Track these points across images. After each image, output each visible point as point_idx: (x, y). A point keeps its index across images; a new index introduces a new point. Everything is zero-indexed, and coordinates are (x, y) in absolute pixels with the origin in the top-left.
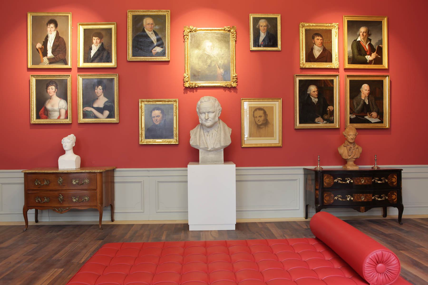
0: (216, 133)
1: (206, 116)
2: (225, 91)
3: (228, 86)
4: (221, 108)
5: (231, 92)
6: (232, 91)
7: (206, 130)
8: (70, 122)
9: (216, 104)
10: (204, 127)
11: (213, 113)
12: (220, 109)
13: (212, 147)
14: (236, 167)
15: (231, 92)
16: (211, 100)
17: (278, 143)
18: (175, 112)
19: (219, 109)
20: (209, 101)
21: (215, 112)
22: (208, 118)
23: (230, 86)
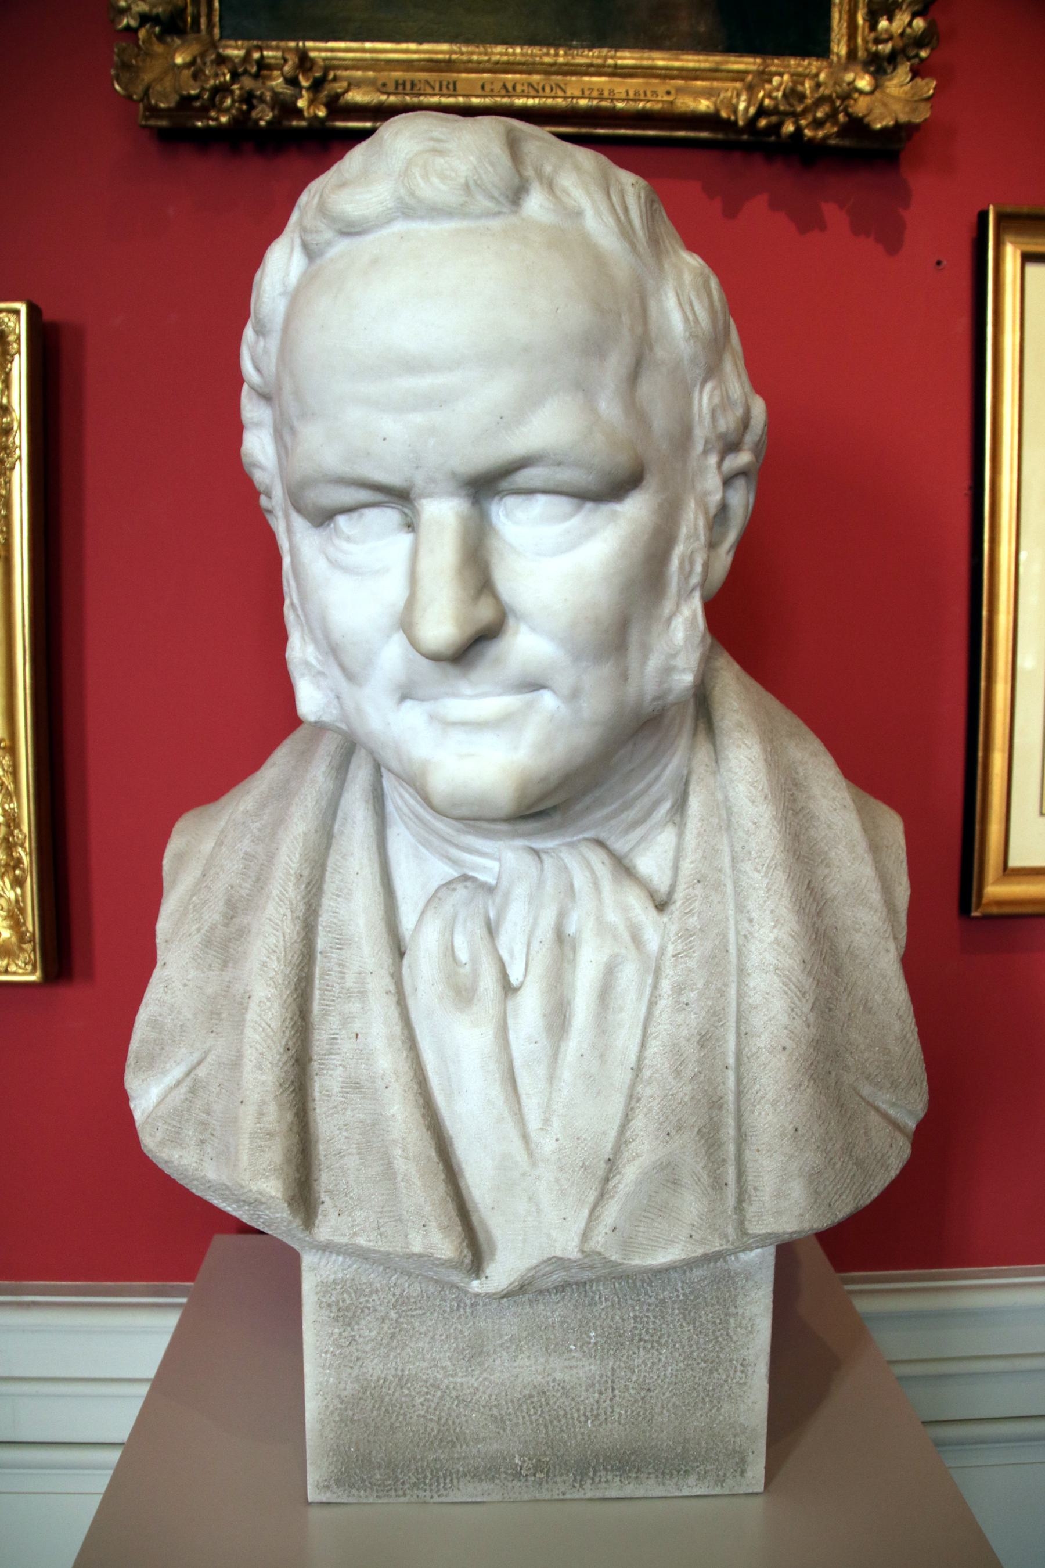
0: (636, 939)
1: (425, 564)
2: (731, 211)
3: (789, 128)
4: (759, 408)
5: (822, 226)
6: (834, 214)
7: (454, 862)
8: (17, 312)
9: (671, 302)
10: (398, 797)
11: (608, 508)
12: (745, 423)
13: (568, 1246)
14: (818, 1251)
15: (822, 226)
16: (550, 186)
17: (1014, 862)
18: (703, 505)
19: (727, 423)
20: (516, 194)
21: (651, 482)
22: (485, 613)
23: (818, 124)
